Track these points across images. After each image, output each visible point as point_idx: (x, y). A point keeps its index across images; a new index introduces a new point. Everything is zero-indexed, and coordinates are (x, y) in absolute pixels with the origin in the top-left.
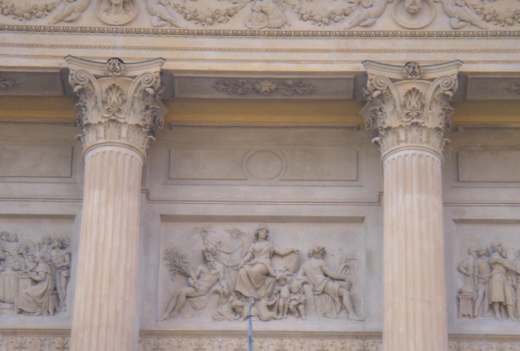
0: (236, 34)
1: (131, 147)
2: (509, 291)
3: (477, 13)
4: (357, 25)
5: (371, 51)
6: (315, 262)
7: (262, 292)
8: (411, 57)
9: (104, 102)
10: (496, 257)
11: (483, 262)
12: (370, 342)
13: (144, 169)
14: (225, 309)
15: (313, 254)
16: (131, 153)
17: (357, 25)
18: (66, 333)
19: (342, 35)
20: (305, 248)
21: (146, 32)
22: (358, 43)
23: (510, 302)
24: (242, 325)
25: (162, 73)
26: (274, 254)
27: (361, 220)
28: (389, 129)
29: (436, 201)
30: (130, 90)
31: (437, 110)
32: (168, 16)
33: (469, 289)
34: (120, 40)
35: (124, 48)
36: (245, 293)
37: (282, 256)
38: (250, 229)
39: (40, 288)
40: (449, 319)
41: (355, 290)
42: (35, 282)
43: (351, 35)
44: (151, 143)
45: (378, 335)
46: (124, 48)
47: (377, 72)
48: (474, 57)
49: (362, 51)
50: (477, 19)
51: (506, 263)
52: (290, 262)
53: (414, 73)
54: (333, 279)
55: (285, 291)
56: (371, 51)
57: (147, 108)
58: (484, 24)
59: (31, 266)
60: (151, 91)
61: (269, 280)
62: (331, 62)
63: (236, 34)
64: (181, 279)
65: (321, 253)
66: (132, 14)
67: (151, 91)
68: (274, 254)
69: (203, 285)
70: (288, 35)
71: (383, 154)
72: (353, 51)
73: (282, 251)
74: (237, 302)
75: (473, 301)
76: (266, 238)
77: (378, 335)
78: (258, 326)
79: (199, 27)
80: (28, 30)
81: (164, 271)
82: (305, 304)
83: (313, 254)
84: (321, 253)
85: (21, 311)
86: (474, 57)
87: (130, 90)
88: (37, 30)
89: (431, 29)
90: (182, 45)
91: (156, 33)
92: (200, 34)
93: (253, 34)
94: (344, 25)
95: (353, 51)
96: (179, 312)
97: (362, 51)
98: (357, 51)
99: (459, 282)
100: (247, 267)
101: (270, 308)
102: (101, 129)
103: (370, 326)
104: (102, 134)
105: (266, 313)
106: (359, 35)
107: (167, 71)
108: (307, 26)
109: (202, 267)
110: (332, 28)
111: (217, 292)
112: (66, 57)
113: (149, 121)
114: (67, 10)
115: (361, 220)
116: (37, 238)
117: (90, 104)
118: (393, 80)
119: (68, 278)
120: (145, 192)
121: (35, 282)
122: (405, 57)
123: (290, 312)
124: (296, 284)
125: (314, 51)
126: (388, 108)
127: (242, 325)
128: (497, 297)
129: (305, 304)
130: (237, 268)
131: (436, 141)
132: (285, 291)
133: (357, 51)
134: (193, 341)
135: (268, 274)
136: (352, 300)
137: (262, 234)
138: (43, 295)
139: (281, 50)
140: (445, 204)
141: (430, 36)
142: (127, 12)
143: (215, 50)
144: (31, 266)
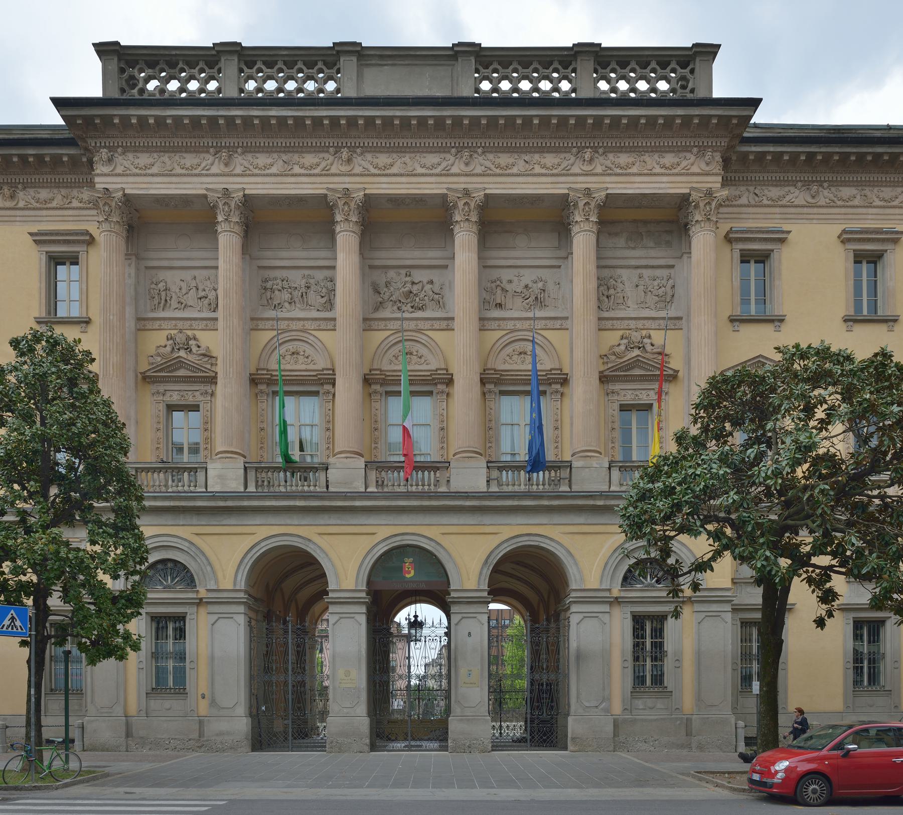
0: (395, 175)
1: (354, 232)
2: (503, 298)
3: (493, 164)
4: (443, 170)
5: (449, 183)
6: (429, 286)
7: (409, 300)
8: (347, 186)
9: (343, 210)
10: (498, 282)
11: (494, 285)
12: (450, 322)
13: (362, 244)
14: (395, 308)
15: (428, 283)
16: (354, 235)
17: (443, 170)
18: (334, 319)
19: (437, 175)
20: (425, 281)
21: (357, 175)
22: (443, 179)
23: (503, 303)
24: (399, 315)
25: (365, 195)
26: (413, 283)
27: (559, 267)
28: (457, 221)
29: (475, 256)
30: (352, 205)
31: (476, 213)
32: (366, 167)
33: (488, 298)
34: (347, 179)
35: (349, 183)
36: (402, 301)
37: (416, 284)
38: (403, 272)
39: (324, 300)
40: (480, 311)
41: (444, 299)
42: (322, 297)
43: (441, 175)
44: (362, 231)
45: (453, 319)
46: (349, 183)
47: (212, 194)
48: (491, 186)
49: (446, 183)
50: (492, 167)
51: (502, 285)
52: (419, 286)
53: (466, 194)
54: (436, 294)
55: (417, 299)
56: (449, 183)
57: (241, 213)
58: (495, 169)
59: (320, 289)
60: (361, 204)
61: (412, 295)
62: (433, 189)
63: (395, 175)
64: (377, 294)
65: (431, 282)
66: (352, 166)
67: (361, 204)
68: (413, 283)
69: (386, 297)
70: (415, 175)
71: (573, 234)
72: (442, 183)
73: (416, 282)
74: (399, 305)
75: (489, 302)
76: (410, 276)
77: (453, 319)
78: (406, 315)
79: (379, 172)
80: (626, 175)
81: (371, 291)
82: (425, 305)
83: (428, 283)
84: (431, 282)
85: (318, 310)
86: (491, 186)
87: (472, 205)
88: (314, 175)
89: (474, 172)
90: (538, 181)
91: (362, 175)
92: (379, 175)
93: (401, 175)
94: (438, 171)
95: (442, 183)
96: (378, 310)
97: (446, 183)
98: (444, 183)
99: (484, 295)
100: (403, 289)
101: (412, 307)
102: (223, 224)
103: (450, 315)
104: (703, 225)
105: (411, 310)
106: (445, 175)
107: (249, 195)
108: (423, 171)
109: (385, 289)
110: (434, 171)
111: (391, 301)
112: (448, 189)
113: (361, 220)
114: (686, 165)
115: (559, 267)
116: (322, 277)
117: (337, 212)
118: (459, 198)
119: (334, 295)
120: (361, 254)
121: (322, 297)
122: (463, 186)
123: (420, 309)
124: (422, 296)
125: (426, 183)
126: (456, 212)
127: (399, 315)
128: (499, 301)
129: (425, 305)
130: (399, 289)
131: (475, 228)
132: (417, 299)
133: (444, 183)
134: (611, 322)
135: (411, 292)
136: (444, 304)
137: (408, 274)
138: (325, 303)
139: (413, 183)
140: (479, 258)
141: (473, 175)
142: (349, 165)
143: (386, 183)
144: (320, 289)
